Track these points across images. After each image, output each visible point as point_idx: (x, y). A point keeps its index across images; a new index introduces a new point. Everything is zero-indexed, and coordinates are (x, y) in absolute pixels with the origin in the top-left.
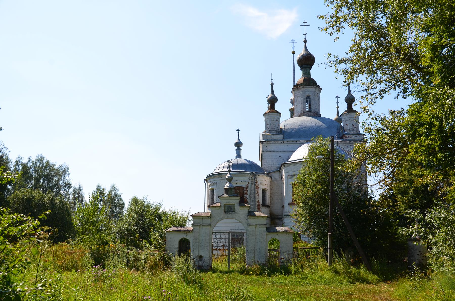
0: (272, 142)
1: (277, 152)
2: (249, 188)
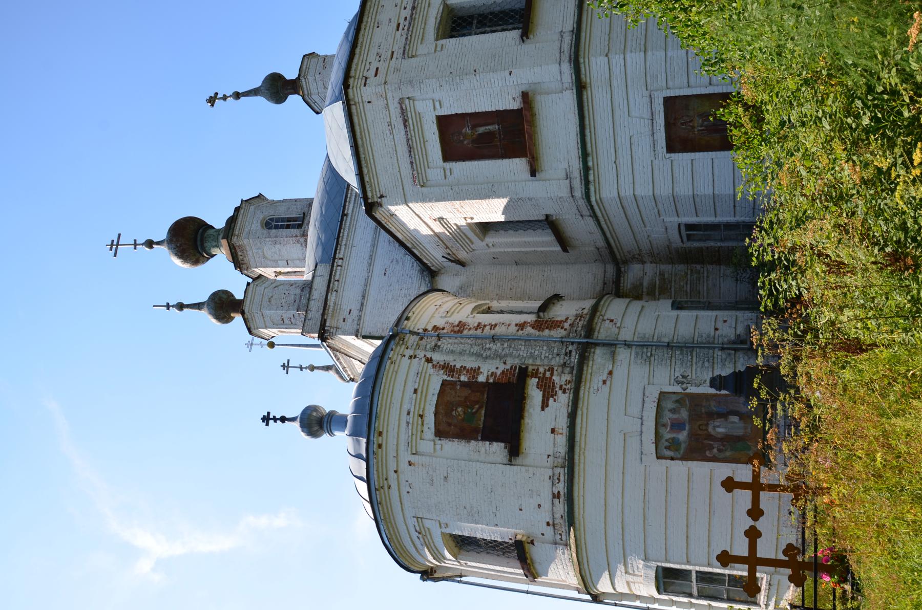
0: (332, 298)
1: (367, 283)
2: (450, 359)
